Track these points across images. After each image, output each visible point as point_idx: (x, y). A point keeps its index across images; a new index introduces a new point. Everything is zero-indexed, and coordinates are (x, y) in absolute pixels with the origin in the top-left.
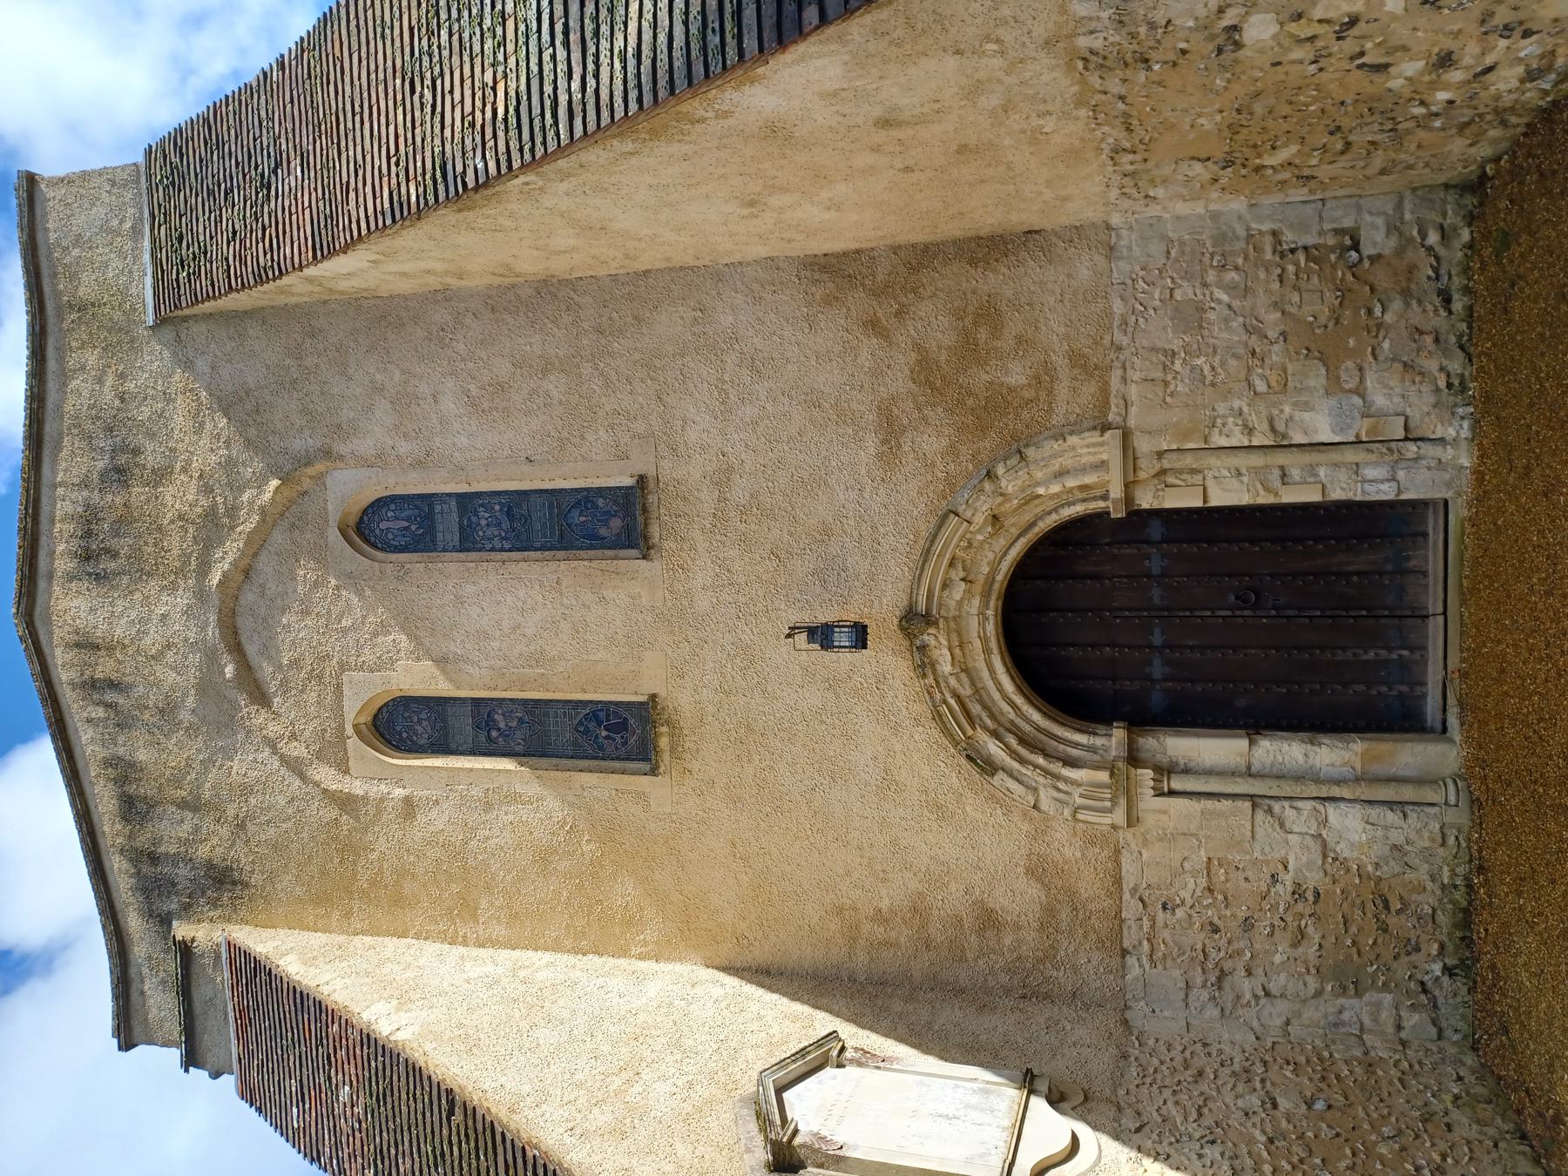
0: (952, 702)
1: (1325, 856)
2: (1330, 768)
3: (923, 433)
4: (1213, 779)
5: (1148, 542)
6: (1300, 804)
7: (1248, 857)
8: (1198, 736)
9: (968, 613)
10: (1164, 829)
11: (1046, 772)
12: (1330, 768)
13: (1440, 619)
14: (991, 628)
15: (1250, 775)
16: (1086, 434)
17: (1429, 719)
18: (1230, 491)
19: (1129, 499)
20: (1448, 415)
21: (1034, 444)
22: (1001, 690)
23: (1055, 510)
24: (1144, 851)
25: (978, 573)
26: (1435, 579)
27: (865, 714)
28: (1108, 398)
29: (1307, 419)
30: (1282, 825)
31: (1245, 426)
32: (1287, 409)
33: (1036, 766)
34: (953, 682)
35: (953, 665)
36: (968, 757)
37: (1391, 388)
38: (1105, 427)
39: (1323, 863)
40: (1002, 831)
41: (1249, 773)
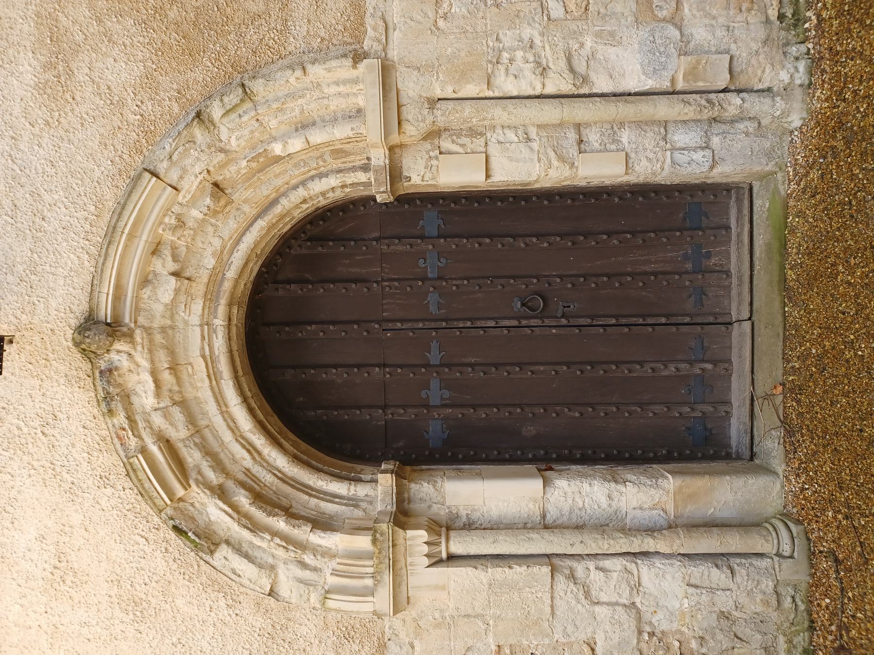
0: (154, 449)
1: (640, 632)
2: (638, 512)
3: (105, 55)
4: (502, 536)
5: (422, 237)
6: (607, 563)
7: (547, 641)
8: (481, 476)
9: (186, 323)
10: (441, 611)
11: (288, 540)
12: (638, 513)
13: (747, 325)
14: (220, 343)
15: (546, 527)
16: (334, 63)
17: (734, 443)
18: (517, 161)
19: (395, 173)
20: (779, 56)
21: (263, 76)
22: (233, 427)
23: (303, 183)
24: (417, 643)
25: (199, 267)
26: (740, 279)
27: (25, 472)
28: (362, 18)
29: (613, 57)
30: (587, 594)
31: (538, 64)
32: (589, 43)
33: (275, 534)
34: (158, 420)
35: (158, 394)
36: (176, 529)
37: (714, 18)
38: (358, 57)
39: (638, 643)
40: (228, 631)
41: (546, 526)
